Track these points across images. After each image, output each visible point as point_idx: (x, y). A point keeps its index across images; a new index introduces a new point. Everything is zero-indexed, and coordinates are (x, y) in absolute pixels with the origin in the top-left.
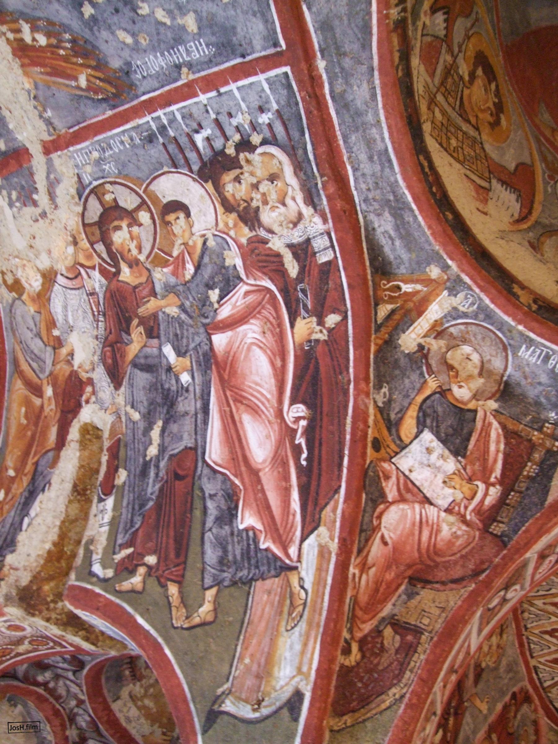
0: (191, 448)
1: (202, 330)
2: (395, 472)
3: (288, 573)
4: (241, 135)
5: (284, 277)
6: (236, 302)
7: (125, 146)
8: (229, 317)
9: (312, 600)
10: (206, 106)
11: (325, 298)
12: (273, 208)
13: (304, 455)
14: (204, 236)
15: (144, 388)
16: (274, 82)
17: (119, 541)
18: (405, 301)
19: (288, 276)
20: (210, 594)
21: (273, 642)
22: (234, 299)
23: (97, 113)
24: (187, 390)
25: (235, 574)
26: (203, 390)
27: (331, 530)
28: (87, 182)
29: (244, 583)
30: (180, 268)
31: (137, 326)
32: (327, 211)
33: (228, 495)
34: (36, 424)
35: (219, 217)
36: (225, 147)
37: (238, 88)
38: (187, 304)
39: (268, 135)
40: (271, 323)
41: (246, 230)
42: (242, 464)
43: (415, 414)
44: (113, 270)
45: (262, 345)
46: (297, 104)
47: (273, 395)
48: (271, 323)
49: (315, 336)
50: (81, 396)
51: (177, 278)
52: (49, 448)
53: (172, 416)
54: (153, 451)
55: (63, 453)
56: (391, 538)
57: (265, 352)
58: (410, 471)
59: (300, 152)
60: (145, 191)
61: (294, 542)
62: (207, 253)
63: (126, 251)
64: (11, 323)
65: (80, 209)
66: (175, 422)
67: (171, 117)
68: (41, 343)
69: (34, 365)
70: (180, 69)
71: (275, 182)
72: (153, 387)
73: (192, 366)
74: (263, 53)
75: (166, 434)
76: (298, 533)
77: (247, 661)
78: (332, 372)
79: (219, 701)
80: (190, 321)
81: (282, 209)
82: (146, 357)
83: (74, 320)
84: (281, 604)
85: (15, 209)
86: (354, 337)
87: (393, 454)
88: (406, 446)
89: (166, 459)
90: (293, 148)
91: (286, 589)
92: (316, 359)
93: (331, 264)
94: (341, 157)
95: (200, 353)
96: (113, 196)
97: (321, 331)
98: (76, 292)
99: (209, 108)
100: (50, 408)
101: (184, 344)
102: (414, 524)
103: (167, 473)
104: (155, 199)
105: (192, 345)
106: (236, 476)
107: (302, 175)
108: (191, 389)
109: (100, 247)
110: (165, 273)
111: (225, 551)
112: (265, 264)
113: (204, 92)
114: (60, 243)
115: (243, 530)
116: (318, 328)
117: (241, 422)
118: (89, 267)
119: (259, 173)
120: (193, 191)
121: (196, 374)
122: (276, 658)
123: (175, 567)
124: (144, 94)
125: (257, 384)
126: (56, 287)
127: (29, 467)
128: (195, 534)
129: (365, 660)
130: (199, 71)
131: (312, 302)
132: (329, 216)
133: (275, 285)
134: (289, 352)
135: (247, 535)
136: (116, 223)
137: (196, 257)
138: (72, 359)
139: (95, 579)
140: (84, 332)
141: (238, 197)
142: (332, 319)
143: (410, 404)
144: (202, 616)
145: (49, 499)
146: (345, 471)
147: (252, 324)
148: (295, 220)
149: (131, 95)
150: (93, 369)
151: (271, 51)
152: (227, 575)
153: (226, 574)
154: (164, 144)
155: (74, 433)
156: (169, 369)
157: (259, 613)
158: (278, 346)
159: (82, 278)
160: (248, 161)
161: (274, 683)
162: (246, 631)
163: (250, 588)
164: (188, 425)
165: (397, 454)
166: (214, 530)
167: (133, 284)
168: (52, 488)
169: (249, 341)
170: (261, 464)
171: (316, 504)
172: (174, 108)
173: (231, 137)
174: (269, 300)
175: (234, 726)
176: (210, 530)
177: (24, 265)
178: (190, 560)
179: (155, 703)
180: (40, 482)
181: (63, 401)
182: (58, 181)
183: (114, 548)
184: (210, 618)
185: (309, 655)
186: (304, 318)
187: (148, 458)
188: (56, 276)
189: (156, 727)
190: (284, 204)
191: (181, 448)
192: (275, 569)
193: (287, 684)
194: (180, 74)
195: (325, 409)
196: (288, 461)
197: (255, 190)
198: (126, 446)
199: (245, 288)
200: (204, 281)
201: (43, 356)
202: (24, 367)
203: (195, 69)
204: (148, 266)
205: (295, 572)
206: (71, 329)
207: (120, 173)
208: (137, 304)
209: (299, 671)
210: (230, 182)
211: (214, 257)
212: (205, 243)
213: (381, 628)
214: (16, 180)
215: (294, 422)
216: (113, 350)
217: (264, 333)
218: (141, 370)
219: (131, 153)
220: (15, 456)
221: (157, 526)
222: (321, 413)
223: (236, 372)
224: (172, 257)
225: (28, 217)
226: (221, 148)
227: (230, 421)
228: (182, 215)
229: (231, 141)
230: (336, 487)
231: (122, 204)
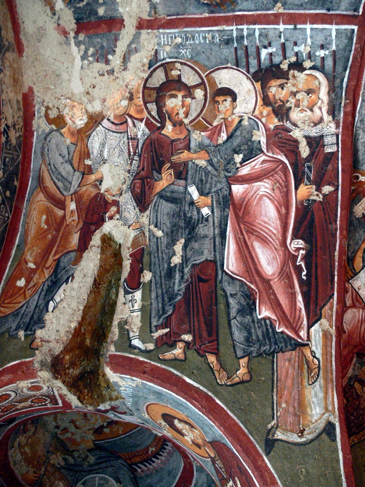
0: (211, 261)
1: (224, 180)
2: (351, 289)
3: (302, 348)
4: (297, 59)
5: (296, 155)
6: (255, 165)
7: (205, 41)
8: (248, 174)
9: (323, 365)
10: (281, 32)
11: (324, 174)
12: (302, 111)
13: (304, 273)
14: (241, 116)
15: (168, 214)
16: (341, 33)
17: (154, 323)
18: (359, 186)
19: (300, 156)
20: (243, 362)
21: (301, 394)
22: (253, 164)
23: (196, 12)
24: (207, 220)
25: (260, 348)
26: (221, 222)
27: (330, 320)
28: (162, 58)
29: (268, 355)
30: (216, 134)
31: (169, 169)
32: (341, 121)
33: (247, 295)
34: (58, 230)
35: (257, 107)
36: (281, 63)
37: (312, 29)
38: (215, 160)
39: (319, 63)
40: (280, 184)
41: (276, 120)
42: (255, 275)
43: (361, 255)
44: (159, 125)
45: (271, 198)
46: (350, 51)
47: (278, 231)
48: (280, 184)
49: (313, 198)
50: (106, 213)
51: (211, 141)
52: (71, 249)
53: (193, 237)
54: (176, 260)
55: (85, 255)
56: (347, 329)
57: (273, 203)
58: (359, 289)
59: (338, 81)
60: (206, 76)
61: (303, 328)
62: (240, 129)
63: (175, 114)
64: (43, 148)
65: (145, 75)
66: (196, 241)
67: (251, 32)
68: (71, 168)
69: (60, 184)
70: (276, 3)
71: (310, 95)
72: (176, 215)
73: (212, 203)
74: (344, 13)
75: (188, 249)
76: (305, 322)
77: (284, 405)
78: (324, 222)
79: (271, 433)
80: (215, 173)
81: (309, 113)
82: (173, 192)
83: (109, 156)
84: (300, 368)
85: (86, 62)
86: (341, 202)
87: (350, 278)
88: (357, 274)
89: (189, 267)
90: (334, 77)
91: (302, 358)
92: (312, 211)
93: (334, 155)
94: (360, 91)
95: (221, 196)
96: (179, 73)
97: (317, 195)
98: (118, 135)
99: (282, 35)
100: (72, 219)
101: (208, 187)
102: (359, 321)
103: (191, 277)
104: (212, 83)
105: (214, 190)
106: (252, 283)
107: (333, 95)
108: (211, 219)
109: (153, 107)
110: (202, 136)
111: (249, 333)
112: (283, 145)
113: (284, 23)
114: (117, 96)
115: (261, 319)
116: (316, 193)
117: (253, 247)
118: (137, 119)
119: (301, 86)
120: (244, 85)
121: (215, 210)
122: (306, 402)
123: (209, 343)
124: (240, 10)
125: (265, 223)
126: (100, 128)
127: (50, 261)
128: (223, 320)
129: (350, 403)
130: (289, 9)
131: (313, 175)
132: (341, 124)
133: (288, 160)
134: (292, 205)
135: (265, 322)
136: (173, 92)
137: (231, 130)
138: (100, 184)
139: (136, 351)
140: (117, 165)
141: (277, 97)
142: (327, 189)
143: (359, 248)
144: (241, 376)
145: (73, 289)
146: (336, 285)
147: (265, 182)
148: (317, 122)
149: (230, 8)
150: (121, 194)
151: (351, 13)
152: (254, 349)
153: (252, 349)
154: (236, 48)
155: (96, 240)
156: (192, 203)
157: (284, 373)
158: (284, 200)
159: (127, 126)
160: (294, 77)
161: (309, 418)
162: (277, 386)
163: (273, 357)
164: (207, 245)
165: (352, 278)
166: (238, 318)
167: (172, 139)
168: (74, 280)
169: (261, 193)
170: (272, 275)
171: (316, 305)
172: (257, 27)
173: (289, 58)
174: (281, 168)
175: (289, 448)
176: (235, 318)
177: (74, 106)
178: (221, 340)
179: (31, 450)
180: (62, 275)
181: (86, 215)
182: (136, 50)
183: (150, 328)
184: (247, 378)
185: (330, 399)
186: (306, 185)
187: (172, 265)
188: (102, 120)
189: (30, 468)
190: (312, 110)
191: (203, 260)
192: (291, 345)
193: (320, 418)
194: (274, 6)
195: (319, 244)
196: (291, 275)
197: (293, 96)
198: (150, 254)
199: (264, 158)
200: (233, 147)
201: (70, 178)
202: (49, 183)
203: (286, 7)
204: (189, 128)
205: (307, 347)
206: (105, 161)
207: (192, 58)
208: (172, 153)
209: (327, 409)
210: (275, 86)
211: (244, 132)
212: (240, 121)
213: (352, 383)
214: (99, 40)
215: (295, 251)
216: (143, 183)
217: (273, 190)
218: (167, 200)
219: (207, 47)
220: (34, 253)
221: (188, 313)
222: (316, 247)
223: (249, 213)
224: (212, 125)
225: (95, 71)
226: (278, 63)
227: (243, 245)
228: (229, 99)
229: (288, 60)
230: (330, 294)
231: (184, 80)
